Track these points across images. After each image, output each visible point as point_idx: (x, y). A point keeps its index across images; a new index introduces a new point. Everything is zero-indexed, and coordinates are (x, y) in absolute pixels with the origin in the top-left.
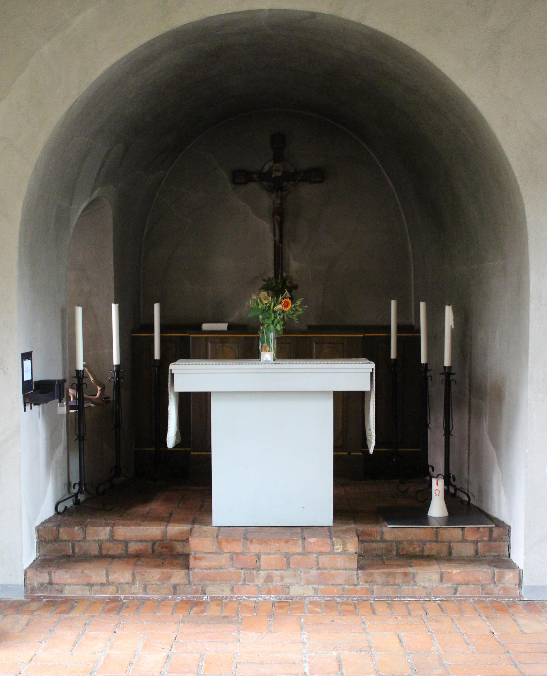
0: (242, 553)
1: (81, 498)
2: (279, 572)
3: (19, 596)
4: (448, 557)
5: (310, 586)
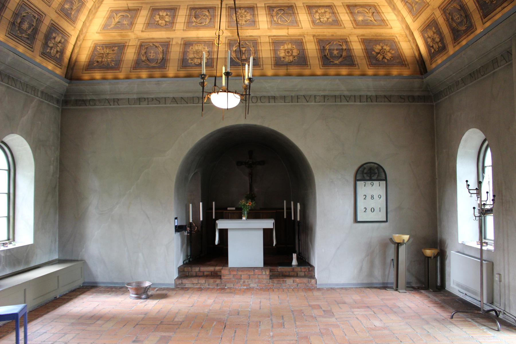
1: (191, 260)
3: (173, 287)
4: (297, 276)
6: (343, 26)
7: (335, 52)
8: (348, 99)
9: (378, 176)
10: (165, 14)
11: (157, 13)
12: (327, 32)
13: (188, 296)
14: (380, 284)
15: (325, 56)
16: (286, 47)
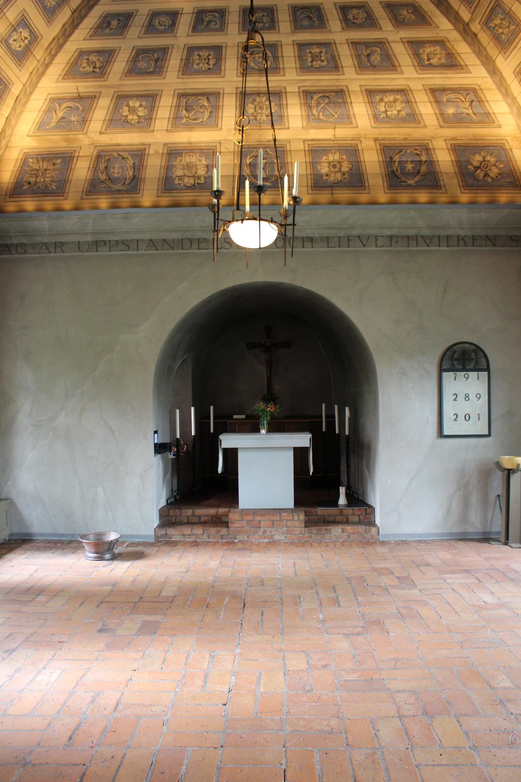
0: (252, 520)
1: (178, 497)
2: (269, 529)
3: (152, 540)
4: (347, 522)
5: (283, 535)
6: (422, 124)
7: (409, 166)
8: (428, 241)
9: (476, 363)
10: (137, 104)
11: (125, 103)
12: (397, 133)
13: (177, 555)
14: (478, 533)
15: (393, 172)
16: (331, 158)
